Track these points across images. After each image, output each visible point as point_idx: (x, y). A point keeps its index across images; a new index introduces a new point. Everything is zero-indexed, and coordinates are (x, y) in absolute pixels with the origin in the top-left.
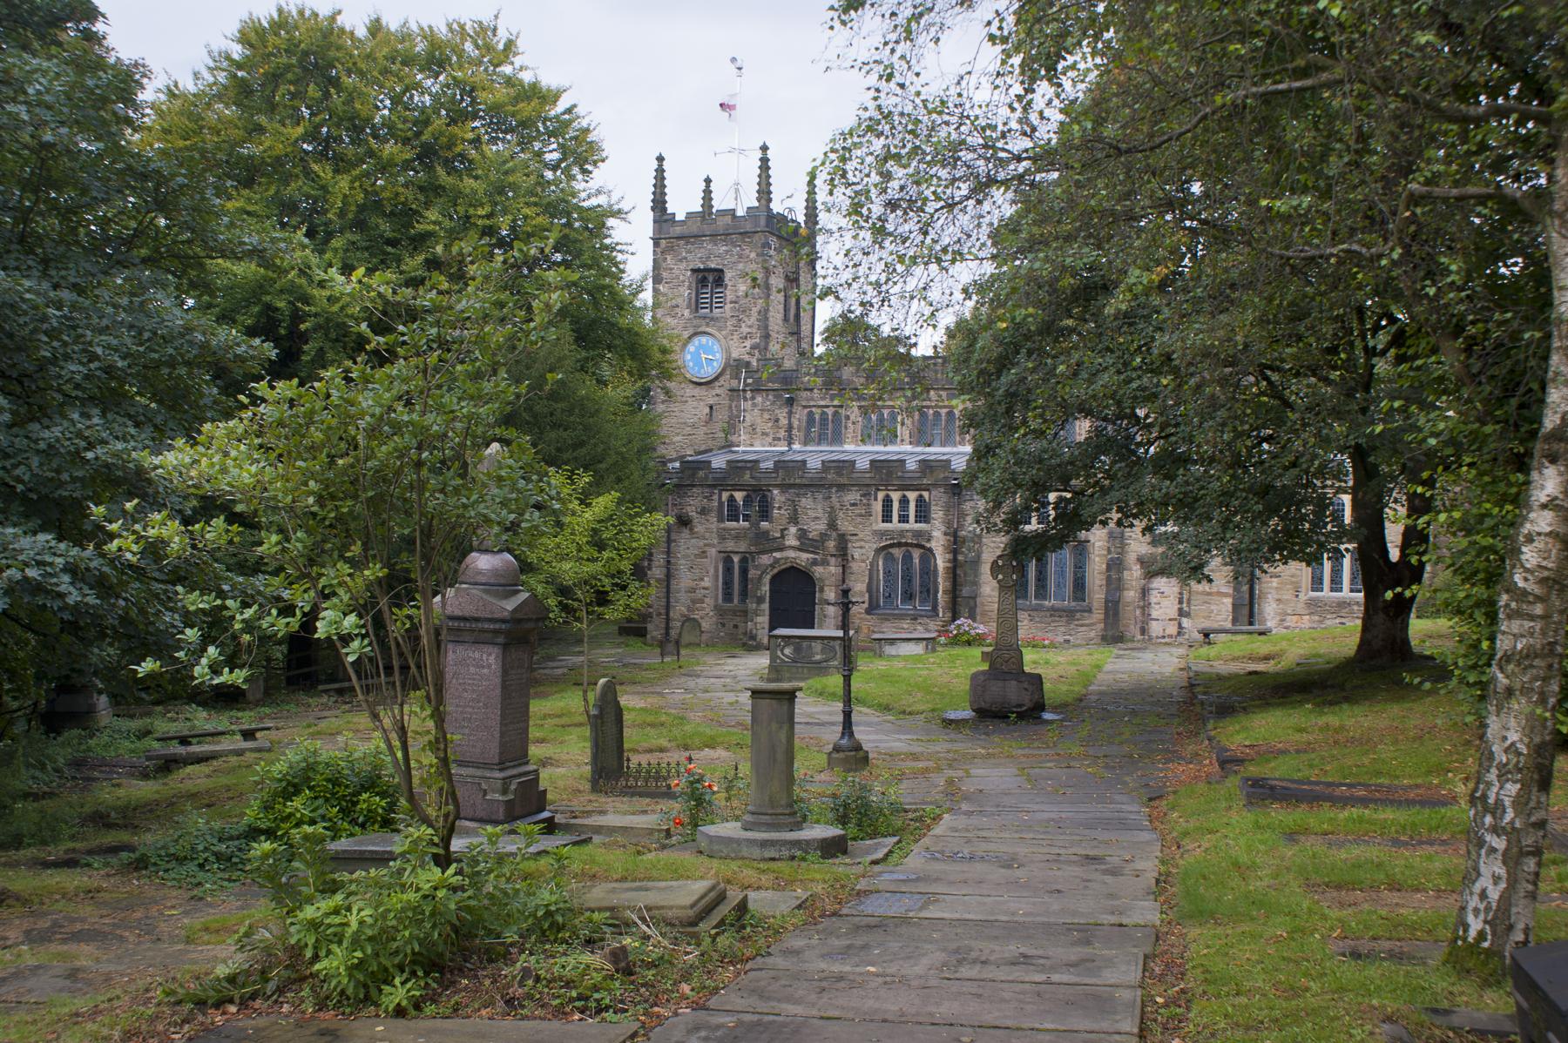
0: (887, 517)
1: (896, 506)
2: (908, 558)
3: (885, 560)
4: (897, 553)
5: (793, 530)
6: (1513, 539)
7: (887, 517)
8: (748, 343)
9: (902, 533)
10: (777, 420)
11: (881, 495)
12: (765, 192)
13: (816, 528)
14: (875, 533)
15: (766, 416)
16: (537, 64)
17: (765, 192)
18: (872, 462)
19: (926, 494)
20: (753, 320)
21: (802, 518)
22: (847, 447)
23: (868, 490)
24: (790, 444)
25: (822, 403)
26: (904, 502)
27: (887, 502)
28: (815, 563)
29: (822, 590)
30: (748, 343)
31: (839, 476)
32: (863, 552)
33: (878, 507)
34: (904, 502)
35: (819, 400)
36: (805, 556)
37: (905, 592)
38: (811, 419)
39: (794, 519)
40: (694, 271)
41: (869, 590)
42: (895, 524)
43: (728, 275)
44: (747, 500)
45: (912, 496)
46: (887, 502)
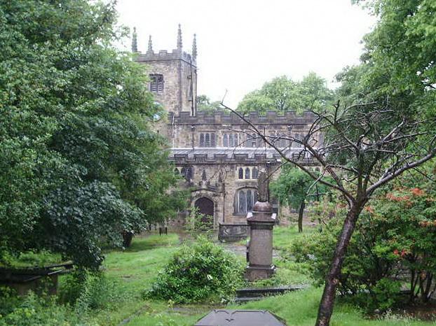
0: (241, 177)
1: (244, 172)
2: (249, 193)
3: (240, 193)
4: (245, 191)
5: (204, 182)
6: (8, 270)
7: (241, 177)
8: (173, 105)
9: (247, 183)
10: (188, 137)
11: (238, 168)
12: (180, 44)
13: (213, 182)
14: (236, 183)
15: (183, 135)
16: (270, 81)
17: (180, 44)
18: (215, 155)
19: (256, 167)
20: (176, 96)
21: (208, 178)
22: (218, 148)
23: (232, 165)
24: (193, 147)
25: (207, 130)
26: (248, 170)
27: (241, 171)
28: (214, 195)
29: (216, 206)
30: (173, 105)
31: (221, 161)
32: (232, 190)
33: (237, 173)
34: (248, 170)
35: (205, 129)
36: (209, 193)
37: (248, 206)
38: (202, 136)
39: (204, 177)
40: (150, 75)
41: (234, 206)
42: (244, 179)
43: (165, 77)
44: (183, 171)
45: (251, 168)
46: (241, 171)
